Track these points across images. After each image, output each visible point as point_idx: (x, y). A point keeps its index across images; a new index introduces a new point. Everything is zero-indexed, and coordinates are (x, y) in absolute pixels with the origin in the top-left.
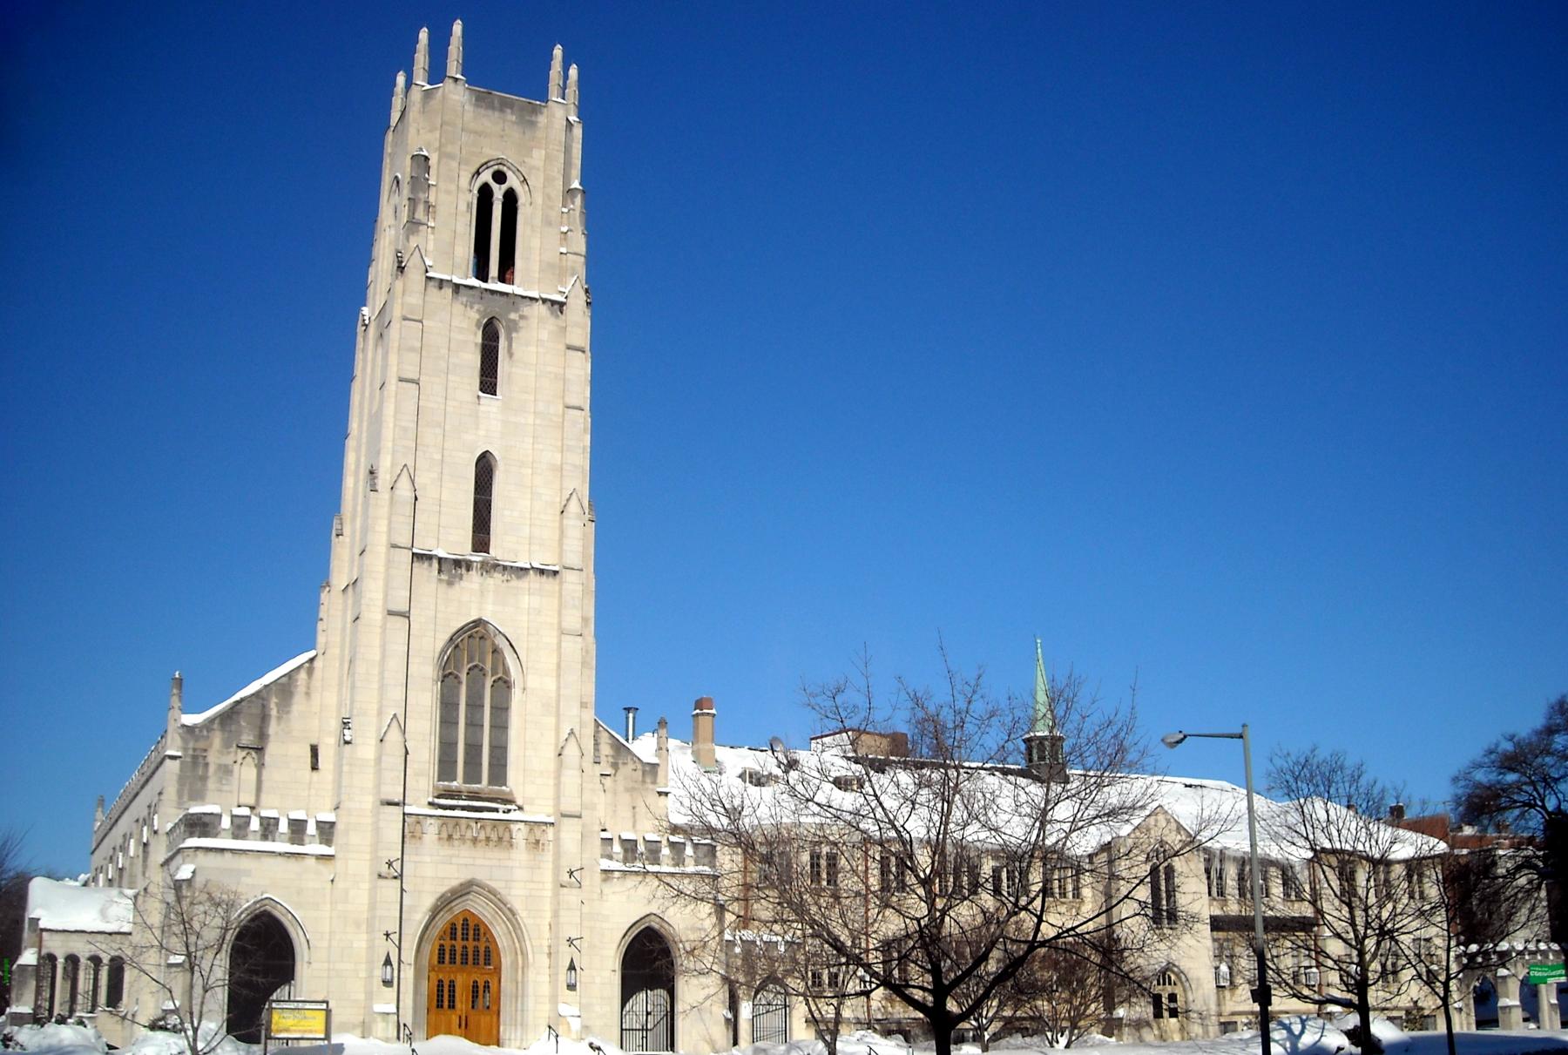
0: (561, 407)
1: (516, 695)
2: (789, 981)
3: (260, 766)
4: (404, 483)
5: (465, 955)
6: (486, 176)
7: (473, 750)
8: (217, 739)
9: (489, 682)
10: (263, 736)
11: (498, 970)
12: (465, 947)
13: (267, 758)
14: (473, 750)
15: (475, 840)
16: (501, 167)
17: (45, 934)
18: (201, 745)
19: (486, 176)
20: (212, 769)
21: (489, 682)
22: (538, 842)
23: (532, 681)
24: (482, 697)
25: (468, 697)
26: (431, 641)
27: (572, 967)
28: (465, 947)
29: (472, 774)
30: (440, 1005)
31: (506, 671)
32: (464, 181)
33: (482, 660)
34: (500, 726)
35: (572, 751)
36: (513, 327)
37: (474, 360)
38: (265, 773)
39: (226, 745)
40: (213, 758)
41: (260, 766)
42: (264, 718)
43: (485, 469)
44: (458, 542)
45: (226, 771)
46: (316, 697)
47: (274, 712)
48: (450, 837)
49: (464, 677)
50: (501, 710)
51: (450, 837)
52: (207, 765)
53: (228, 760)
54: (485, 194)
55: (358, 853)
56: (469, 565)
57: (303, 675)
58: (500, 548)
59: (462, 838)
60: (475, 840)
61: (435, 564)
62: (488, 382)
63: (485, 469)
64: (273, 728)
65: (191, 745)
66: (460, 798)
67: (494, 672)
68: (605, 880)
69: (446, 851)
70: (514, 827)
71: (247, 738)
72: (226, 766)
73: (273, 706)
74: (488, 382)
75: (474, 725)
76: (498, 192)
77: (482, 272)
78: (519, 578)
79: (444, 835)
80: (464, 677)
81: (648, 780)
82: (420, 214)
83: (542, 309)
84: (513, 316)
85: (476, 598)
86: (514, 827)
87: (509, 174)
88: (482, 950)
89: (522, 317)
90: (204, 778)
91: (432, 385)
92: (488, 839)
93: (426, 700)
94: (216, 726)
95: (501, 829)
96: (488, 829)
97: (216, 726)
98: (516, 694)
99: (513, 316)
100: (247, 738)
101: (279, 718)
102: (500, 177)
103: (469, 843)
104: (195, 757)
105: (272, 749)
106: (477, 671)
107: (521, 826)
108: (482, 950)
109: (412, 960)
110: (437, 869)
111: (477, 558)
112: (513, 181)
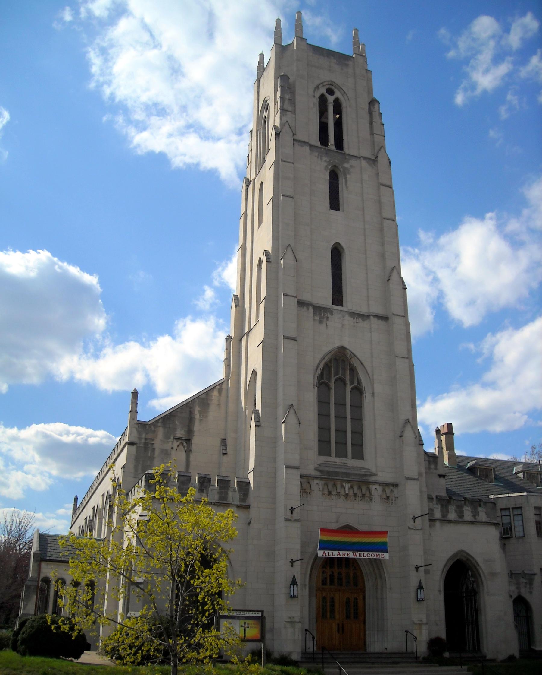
1: (367, 398)
2: (204, 617)
3: (188, 452)
5: (340, 579)
7: (341, 431)
8: (160, 432)
9: (349, 388)
10: (190, 432)
11: (363, 591)
12: (340, 574)
13: (193, 447)
14: (341, 431)
16: (331, 87)
17: (407, 356)
18: (150, 436)
19: (323, 91)
20: (157, 452)
21: (349, 388)
22: (388, 498)
23: (378, 388)
24: (344, 398)
25: (335, 399)
26: (314, 359)
27: (420, 587)
28: (340, 574)
30: (324, 616)
31: (359, 382)
32: (311, 91)
33: (344, 375)
34: (358, 419)
36: (346, 172)
37: (324, 188)
38: (192, 456)
39: (167, 437)
40: (158, 444)
41: (188, 452)
42: (191, 420)
43: (337, 253)
44: (324, 297)
47: (197, 417)
48: (330, 493)
50: (358, 407)
51: (330, 493)
52: (154, 449)
53: (168, 446)
54: (323, 100)
56: (331, 311)
57: (215, 393)
58: (353, 299)
59: (338, 494)
60: (347, 495)
61: (311, 309)
62: (335, 203)
63: (337, 253)
64: (197, 427)
65: (143, 436)
67: (352, 383)
68: (430, 526)
70: (373, 487)
71: (180, 433)
72: (166, 450)
73: (196, 412)
74: (335, 203)
75: (340, 417)
76: (331, 99)
77: (324, 140)
78: (363, 320)
79: (326, 492)
80: (332, 385)
81: (432, 466)
83: (364, 163)
84: (346, 165)
86: (373, 487)
87: (336, 90)
88: (336, 575)
89: (351, 166)
92: (355, 495)
93: (311, 396)
94: (160, 424)
95: (364, 489)
96: (355, 488)
97: (160, 424)
99: (346, 165)
100: (180, 433)
101: (201, 420)
102: (330, 92)
103: (342, 497)
104: (146, 444)
105: (196, 440)
107: (377, 486)
108: (336, 575)
112: (338, 94)
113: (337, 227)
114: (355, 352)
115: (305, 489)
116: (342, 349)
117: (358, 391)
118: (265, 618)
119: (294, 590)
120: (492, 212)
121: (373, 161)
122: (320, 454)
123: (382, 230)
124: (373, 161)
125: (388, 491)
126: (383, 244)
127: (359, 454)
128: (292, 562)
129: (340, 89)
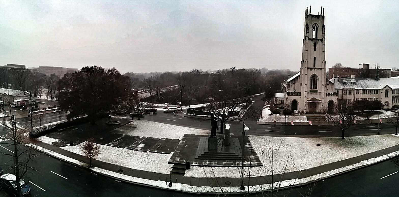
0: (308, 44)
3: (295, 85)
4: (306, 61)
6: (314, 25)
8: (291, 83)
10: (295, 82)
15: (314, 94)
20: (290, 86)
29: (314, 88)
35: (323, 86)
39: (292, 83)
41: (295, 85)
43: (315, 58)
44: (312, 67)
45: (292, 86)
46: (300, 79)
49: (313, 79)
55: (304, 94)
57: (299, 77)
58: (316, 67)
59: (313, 94)
62: (315, 50)
63: (315, 58)
66: (312, 86)
69: (311, 95)
74: (315, 50)
75: (314, 84)
76: (316, 27)
82: (307, 32)
85: (314, 72)
90: (290, 86)
91: (309, 50)
93: (309, 82)
98: (318, 80)
100: (294, 83)
105: (296, 83)
106: (314, 79)
109: (313, 36)
110: (311, 96)
111: (314, 68)
112: (317, 25)
113: (315, 54)
114: (304, 16)
115: (308, 94)
116: (314, 74)
117: (317, 80)
118: (324, 16)
119: (305, 106)
120: (86, 141)
121: (322, 40)
122: (311, 88)
123: (322, 54)
124: (322, 40)
125: (320, 93)
126: (322, 56)
127: (316, 88)
128: (305, 103)
129: (317, 24)
